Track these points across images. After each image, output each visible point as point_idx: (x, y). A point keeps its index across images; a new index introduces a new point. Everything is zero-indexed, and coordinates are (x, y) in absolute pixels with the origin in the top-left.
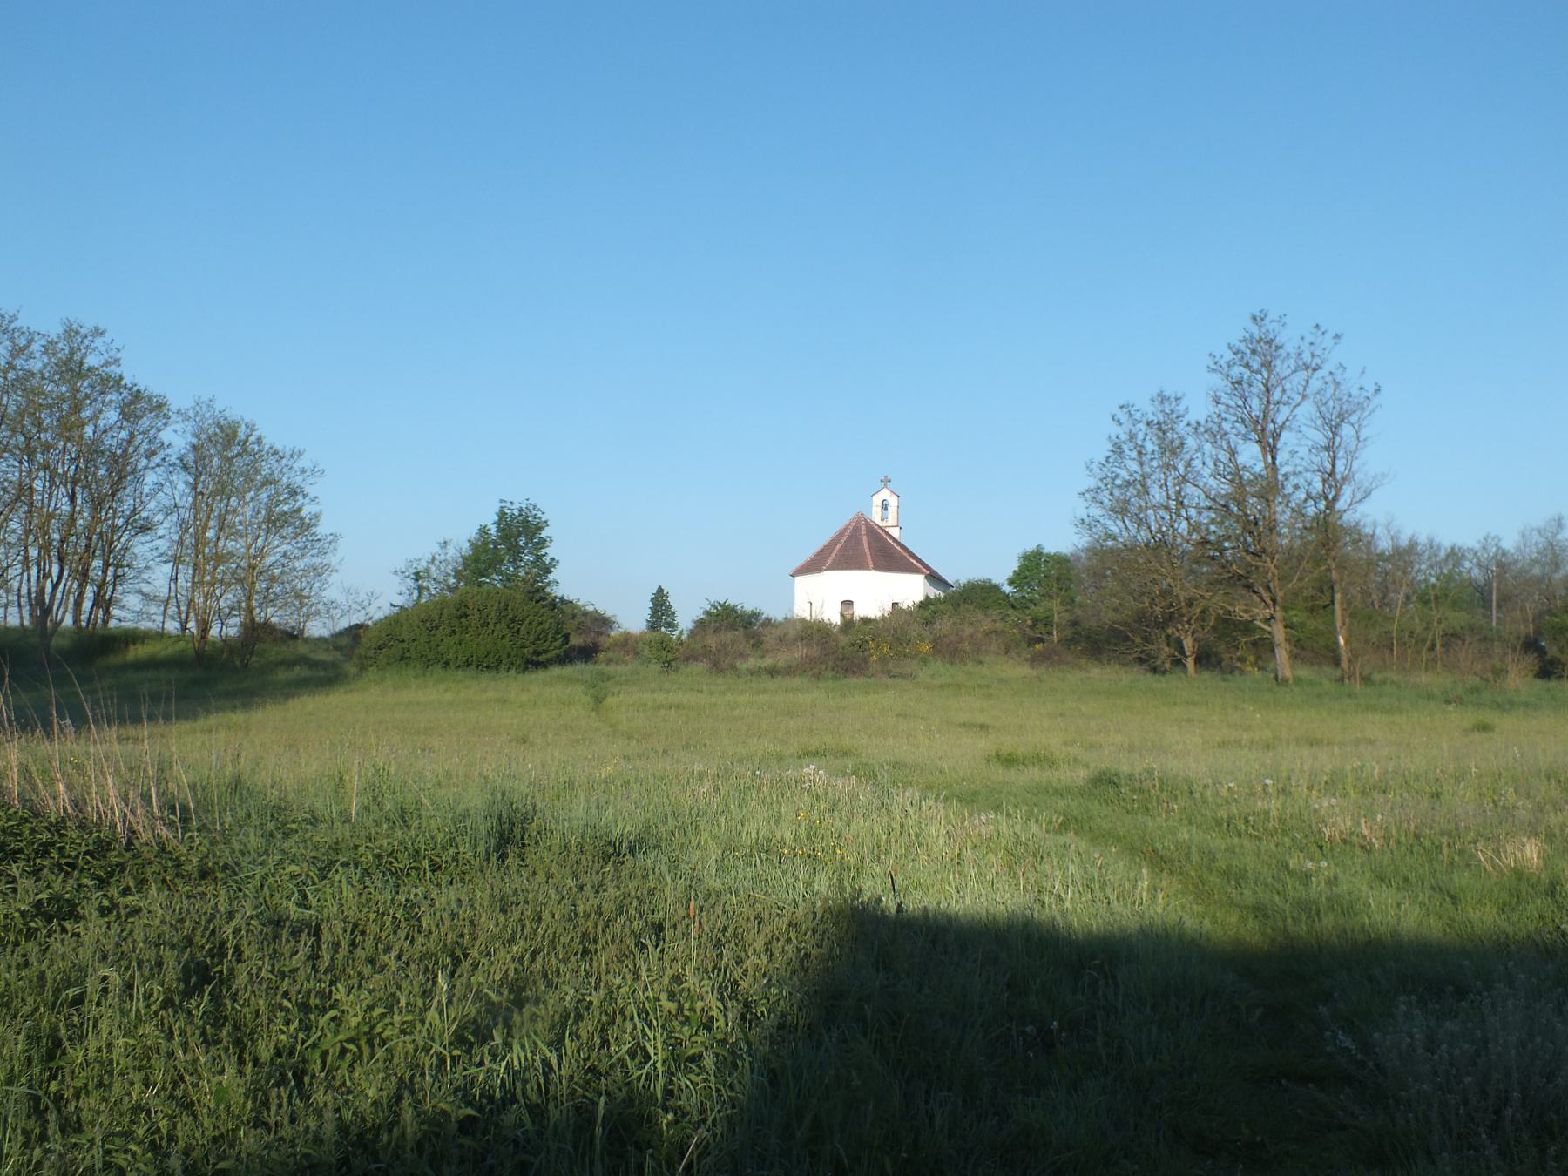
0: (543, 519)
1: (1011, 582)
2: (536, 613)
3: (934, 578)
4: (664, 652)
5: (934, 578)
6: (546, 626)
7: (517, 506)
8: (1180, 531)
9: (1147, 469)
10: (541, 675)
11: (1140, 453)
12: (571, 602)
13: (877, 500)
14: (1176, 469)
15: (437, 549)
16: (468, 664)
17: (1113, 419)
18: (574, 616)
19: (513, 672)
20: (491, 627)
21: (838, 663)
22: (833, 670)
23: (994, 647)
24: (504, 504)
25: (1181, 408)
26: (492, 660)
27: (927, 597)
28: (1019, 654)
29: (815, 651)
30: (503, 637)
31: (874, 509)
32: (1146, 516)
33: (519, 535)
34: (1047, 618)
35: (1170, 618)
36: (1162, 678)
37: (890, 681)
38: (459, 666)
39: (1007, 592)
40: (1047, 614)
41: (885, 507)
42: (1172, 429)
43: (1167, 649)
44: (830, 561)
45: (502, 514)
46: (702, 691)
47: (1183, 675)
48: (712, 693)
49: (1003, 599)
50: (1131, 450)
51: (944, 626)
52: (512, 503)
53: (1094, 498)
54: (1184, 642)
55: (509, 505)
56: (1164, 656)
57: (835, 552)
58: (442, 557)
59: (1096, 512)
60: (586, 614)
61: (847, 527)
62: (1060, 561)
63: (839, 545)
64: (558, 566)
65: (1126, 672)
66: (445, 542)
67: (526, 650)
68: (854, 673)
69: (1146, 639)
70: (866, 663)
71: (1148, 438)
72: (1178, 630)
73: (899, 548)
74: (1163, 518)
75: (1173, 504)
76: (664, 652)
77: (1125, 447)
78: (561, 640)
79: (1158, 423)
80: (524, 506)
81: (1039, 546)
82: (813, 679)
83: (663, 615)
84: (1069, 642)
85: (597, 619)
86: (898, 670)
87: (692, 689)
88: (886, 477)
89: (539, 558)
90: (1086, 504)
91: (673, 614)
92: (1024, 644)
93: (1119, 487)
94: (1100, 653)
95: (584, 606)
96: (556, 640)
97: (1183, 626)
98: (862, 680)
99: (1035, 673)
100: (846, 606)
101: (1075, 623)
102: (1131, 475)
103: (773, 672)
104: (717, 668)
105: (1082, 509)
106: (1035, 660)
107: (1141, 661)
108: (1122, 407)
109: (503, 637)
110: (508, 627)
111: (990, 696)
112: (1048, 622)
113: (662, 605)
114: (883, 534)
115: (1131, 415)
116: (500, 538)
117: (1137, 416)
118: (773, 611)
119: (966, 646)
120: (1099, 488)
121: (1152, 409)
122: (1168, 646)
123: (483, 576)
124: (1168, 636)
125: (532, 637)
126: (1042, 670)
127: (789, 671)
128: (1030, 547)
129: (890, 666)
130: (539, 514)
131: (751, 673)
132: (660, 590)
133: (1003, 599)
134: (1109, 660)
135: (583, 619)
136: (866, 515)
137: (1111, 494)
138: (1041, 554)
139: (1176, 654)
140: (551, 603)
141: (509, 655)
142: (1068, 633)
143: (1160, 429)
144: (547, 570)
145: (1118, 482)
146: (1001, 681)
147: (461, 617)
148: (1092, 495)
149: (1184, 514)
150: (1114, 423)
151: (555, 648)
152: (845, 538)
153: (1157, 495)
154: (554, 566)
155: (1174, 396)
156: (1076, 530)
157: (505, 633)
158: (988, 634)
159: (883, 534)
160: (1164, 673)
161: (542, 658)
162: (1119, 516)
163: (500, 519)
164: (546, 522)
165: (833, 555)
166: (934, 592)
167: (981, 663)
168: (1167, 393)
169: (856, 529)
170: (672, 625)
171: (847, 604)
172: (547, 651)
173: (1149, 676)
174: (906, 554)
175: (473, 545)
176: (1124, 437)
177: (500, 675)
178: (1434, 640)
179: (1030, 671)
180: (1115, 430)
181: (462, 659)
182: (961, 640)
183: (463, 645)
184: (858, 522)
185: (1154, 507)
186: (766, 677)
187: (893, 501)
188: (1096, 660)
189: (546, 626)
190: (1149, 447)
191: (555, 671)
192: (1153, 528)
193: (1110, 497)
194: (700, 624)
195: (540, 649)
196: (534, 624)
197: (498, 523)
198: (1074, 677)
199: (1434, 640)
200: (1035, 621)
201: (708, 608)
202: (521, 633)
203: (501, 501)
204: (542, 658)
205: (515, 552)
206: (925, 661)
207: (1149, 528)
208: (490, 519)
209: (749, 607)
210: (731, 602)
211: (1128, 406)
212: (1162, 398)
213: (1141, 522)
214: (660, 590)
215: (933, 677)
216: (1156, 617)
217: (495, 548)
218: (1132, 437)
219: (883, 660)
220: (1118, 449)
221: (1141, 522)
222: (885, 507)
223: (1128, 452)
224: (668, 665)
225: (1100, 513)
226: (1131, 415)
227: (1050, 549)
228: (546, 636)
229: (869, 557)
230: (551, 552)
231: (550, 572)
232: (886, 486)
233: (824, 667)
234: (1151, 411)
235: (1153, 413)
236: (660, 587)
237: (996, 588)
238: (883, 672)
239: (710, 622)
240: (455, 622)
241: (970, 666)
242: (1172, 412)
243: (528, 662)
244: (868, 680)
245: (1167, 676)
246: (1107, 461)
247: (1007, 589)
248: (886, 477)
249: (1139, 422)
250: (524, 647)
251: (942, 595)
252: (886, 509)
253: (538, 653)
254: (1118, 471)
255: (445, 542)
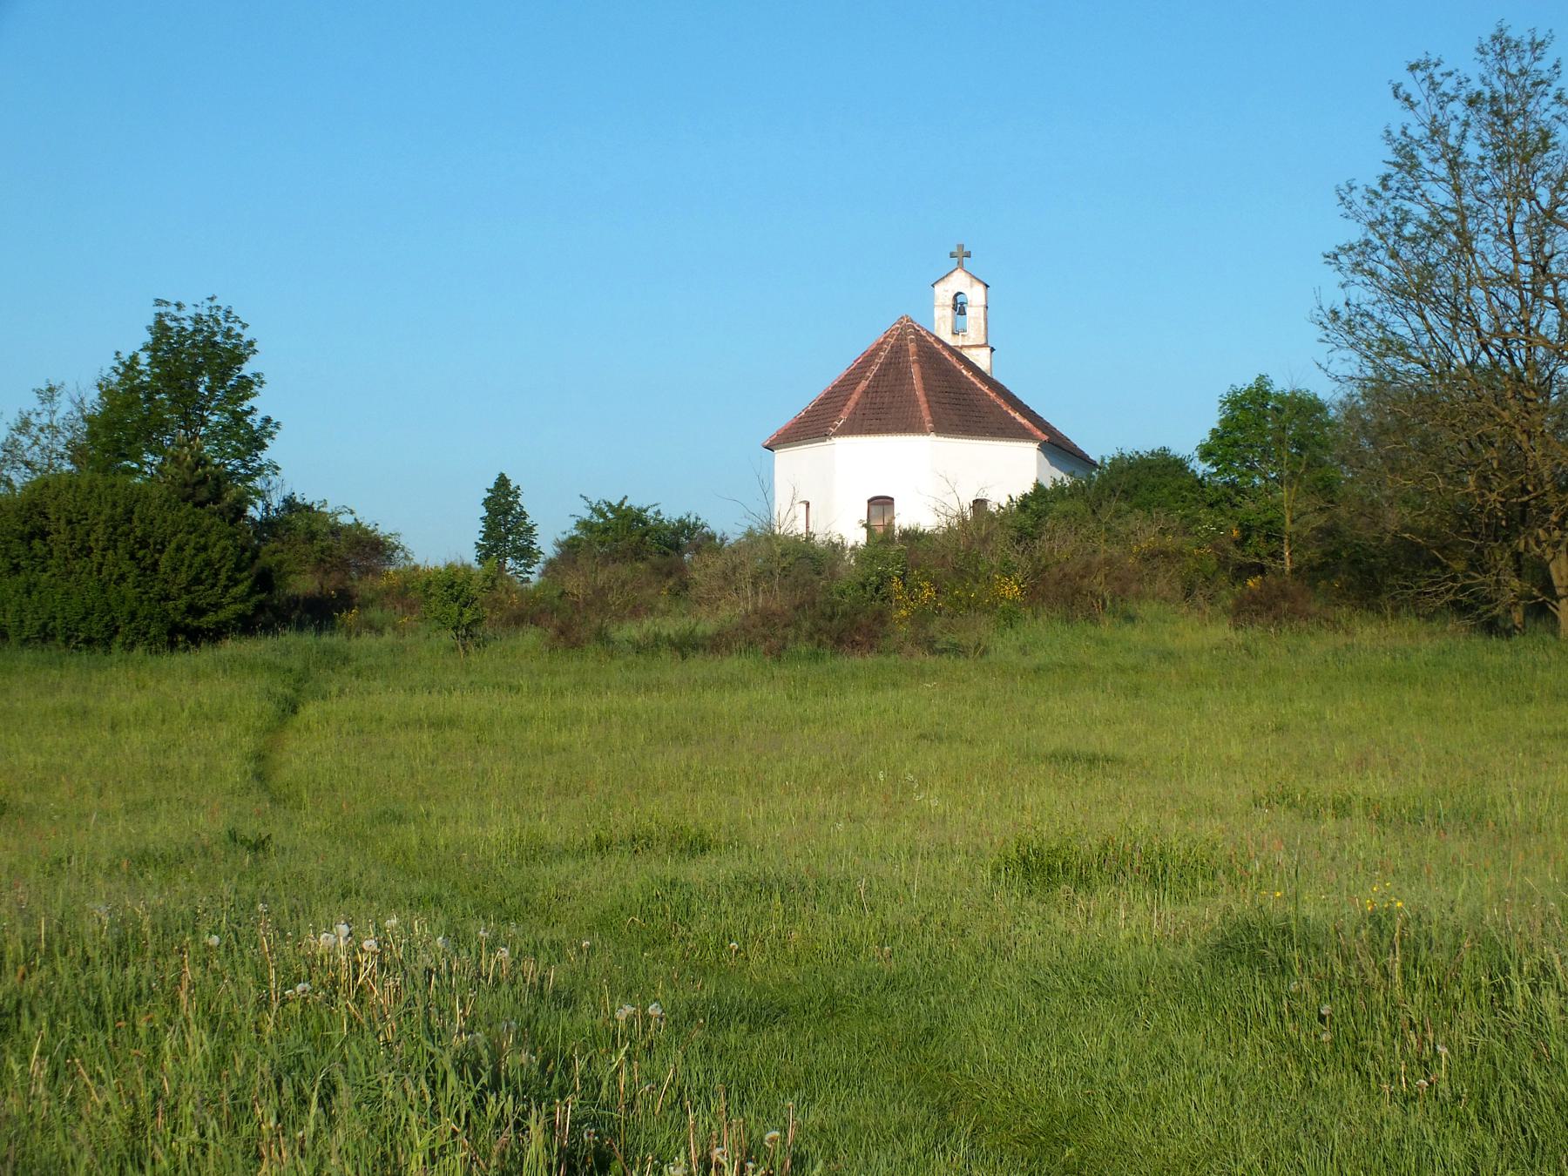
0: (245, 339)
1: (1206, 453)
2: (193, 528)
3: (1057, 448)
4: (456, 607)
5: (1057, 448)
6: (215, 554)
7: (190, 311)
8: (1542, 331)
9: (1468, 200)
10: (204, 656)
11: (1453, 165)
12: (309, 508)
13: (944, 293)
14: (1532, 197)
15: (33, 403)
16: (46, 635)
17: (1396, 96)
18: (312, 536)
19: (139, 651)
20: (96, 557)
21: (822, 623)
22: (810, 637)
23: (1161, 584)
24: (163, 310)
25: (1545, 65)
26: (96, 627)
27: (1039, 487)
28: (1211, 599)
29: (780, 601)
30: (122, 577)
31: (938, 313)
32: (1469, 300)
33: (198, 370)
34: (1270, 522)
35: (1520, 518)
36: (1505, 644)
37: (931, 661)
38: (27, 640)
39: (1200, 474)
40: (1270, 514)
41: (959, 307)
42: (1523, 112)
43: (1515, 583)
44: (844, 417)
45: (160, 329)
46: (519, 689)
47: (1549, 637)
48: (538, 691)
49: (1191, 489)
50: (1435, 160)
51: (1059, 546)
52: (179, 306)
53: (1358, 264)
54: (1552, 567)
55: (172, 310)
56: (1509, 597)
57: (855, 397)
58: (45, 420)
59: (1363, 294)
60: (336, 531)
61: (879, 347)
62: (1305, 408)
63: (864, 384)
64: (278, 435)
65: (1431, 634)
66: (51, 390)
67: (171, 604)
68: (855, 644)
69: (1477, 565)
70: (883, 623)
71: (1471, 133)
72: (1538, 543)
73: (985, 389)
74: (1507, 307)
75: (1525, 271)
76: (456, 607)
77: (1422, 156)
78: (247, 583)
79: (1494, 99)
80: (205, 312)
81: (1262, 377)
82: (768, 660)
83: (509, 531)
84: (1312, 573)
85: (359, 542)
86: (954, 638)
87: (497, 686)
88: (961, 247)
89: (238, 418)
90: (1340, 278)
91: (530, 530)
92: (1223, 579)
93: (1414, 239)
94: (1378, 593)
95: (334, 515)
96: (237, 583)
97: (1547, 530)
98: (871, 660)
99: (1238, 637)
100: (879, 508)
101: (1329, 532)
102: (1434, 214)
103: (685, 646)
104: (568, 637)
105: (1333, 289)
106: (1243, 612)
107: (1461, 609)
108: (1413, 68)
109: (122, 577)
110: (132, 557)
111: (1136, 690)
112: (1272, 532)
113: (506, 513)
114: (953, 360)
115: (1434, 86)
116: (157, 377)
117: (1448, 86)
118: (728, 524)
119: (1098, 584)
120: (1367, 243)
121: (1481, 69)
122: (1519, 576)
123: (126, 457)
124: (1517, 556)
125: (183, 577)
126: (1255, 632)
127: (717, 644)
128: (1244, 380)
129: (935, 627)
130: (237, 329)
131: (639, 649)
132: (502, 482)
133: (1191, 489)
134: (1396, 609)
135: (330, 541)
136: (920, 320)
137: (1394, 255)
138: (1267, 393)
139: (1535, 592)
140: (230, 507)
141: (133, 615)
142: (1313, 554)
143: (1497, 113)
144: (256, 442)
145: (1409, 230)
146: (1166, 656)
147: (32, 536)
148: (1354, 258)
149: (1550, 293)
150: (1398, 103)
151: (235, 600)
152: (875, 368)
153: (1491, 254)
154: (270, 435)
155: (1528, 39)
156: (1321, 334)
157: (125, 568)
158: (1149, 557)
159: (953, 360)
160: (1508, 634)
161: (209, 620)
162: (1413, 303)
163: (157, 340)
164: (251, 344)
165: (851, 404)
166: (1053, 475)
167: (1130, 619)
168: (1513, 34)
169: (898, 351)
170: (526, 553)
171: (881, 504)
172: (217, 606)
173: (1477, 640)
174: (1000, 401)
175: (105, 390)
176: (1417, 132)
177: (115, 658)
178: (975, 653)
179: (1231, 634)
180: (1397, 116)
181: (32, 625)
182: (1087, 571)
183: (35, 597)
184: (901, 337)
185: (1485, 282)
186: (666, 655)
187: (975, 296)
188: (1369, 608)
189: (215, 554)
190: (1472, 150)
191: (230, 647)
192: (1484, 326)
193: (1392, 263)
194: (570, 548)
195: (202, 603)
196: (189, 551)
197: (153, 349)
198: (1319, 645)
199: (975, 653)
200: (1247, 530)
201: (586, 514)
202: (162, 569)
203: (159, 302)
204: (209, 620)
205: (190, 409)
206: (1010, 619)
207: (1476, 325)
208: (134, 339)
209: (672, 512)
210: (635, 502)
211: (1427, 65)
212: (1502, 44)
213: (1460, 316)
214: (502, 482)
215: (1023, 650)
216: (1491, 514)
217: (150, 399)
218: (1437, 131)
219: (921, 618)
220: (1407, 161)
221: (1460, 316)
222: (959, 307)
223: (1428, 166)
224: (468, 632)
225: (1374, 298)
226: (1434, 86)
227: (1281, 384)
228: (216, 574)
229: (924, 406)
230: (262, 404)
231: (263, 446)
232: (960, 265)
233: (791, 632)
234: (1475, 73)
235: (1483, 79)
236: (502, 475)
237: (1179, 465)
238: (917, 643)
239: (589, 544)
240: (18, 548)
241: (1106, 629)
242: (1523, 72)
243: (174, 630)
244: (882, 658)
245: (1516, 638)
246: (1385, 187)
247: (1201, 468)
248: (961, 247)
249: (1452, 99)
250: (167, 598)
251: (1068, 481)
252: (962, 312)
253: (194, 610)
254: (1407, 205)
255: (51, 390)
